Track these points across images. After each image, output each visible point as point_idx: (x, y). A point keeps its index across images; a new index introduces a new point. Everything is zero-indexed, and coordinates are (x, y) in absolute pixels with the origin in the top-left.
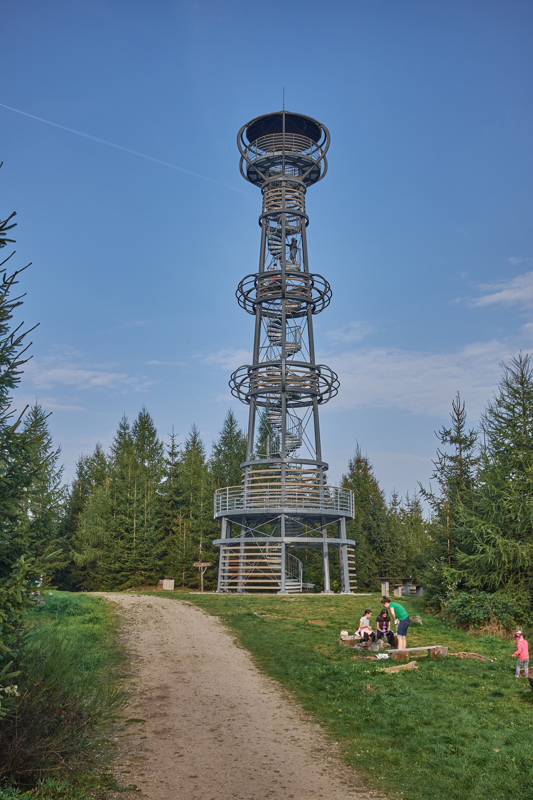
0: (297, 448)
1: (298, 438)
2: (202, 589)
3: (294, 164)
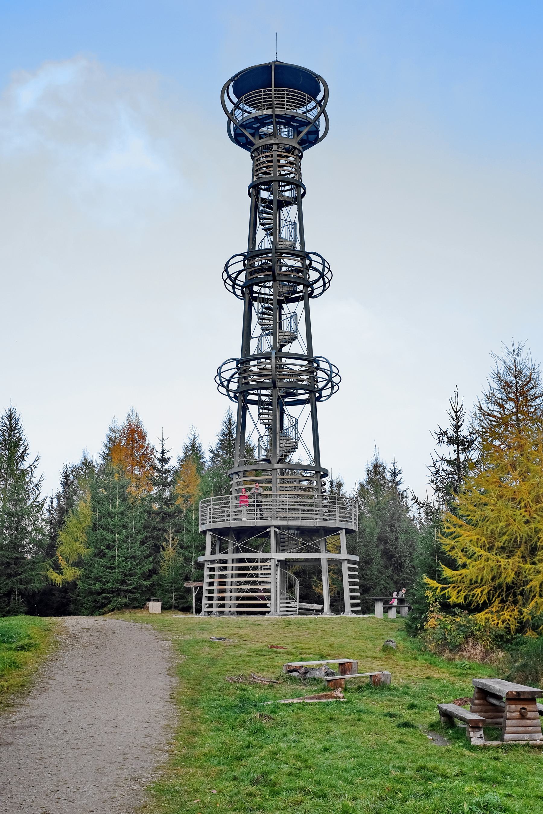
0: (292, 452)
1: (294, 440)
2: (194, 612)
3: (287, 124)
